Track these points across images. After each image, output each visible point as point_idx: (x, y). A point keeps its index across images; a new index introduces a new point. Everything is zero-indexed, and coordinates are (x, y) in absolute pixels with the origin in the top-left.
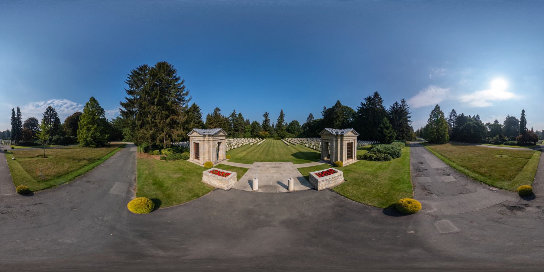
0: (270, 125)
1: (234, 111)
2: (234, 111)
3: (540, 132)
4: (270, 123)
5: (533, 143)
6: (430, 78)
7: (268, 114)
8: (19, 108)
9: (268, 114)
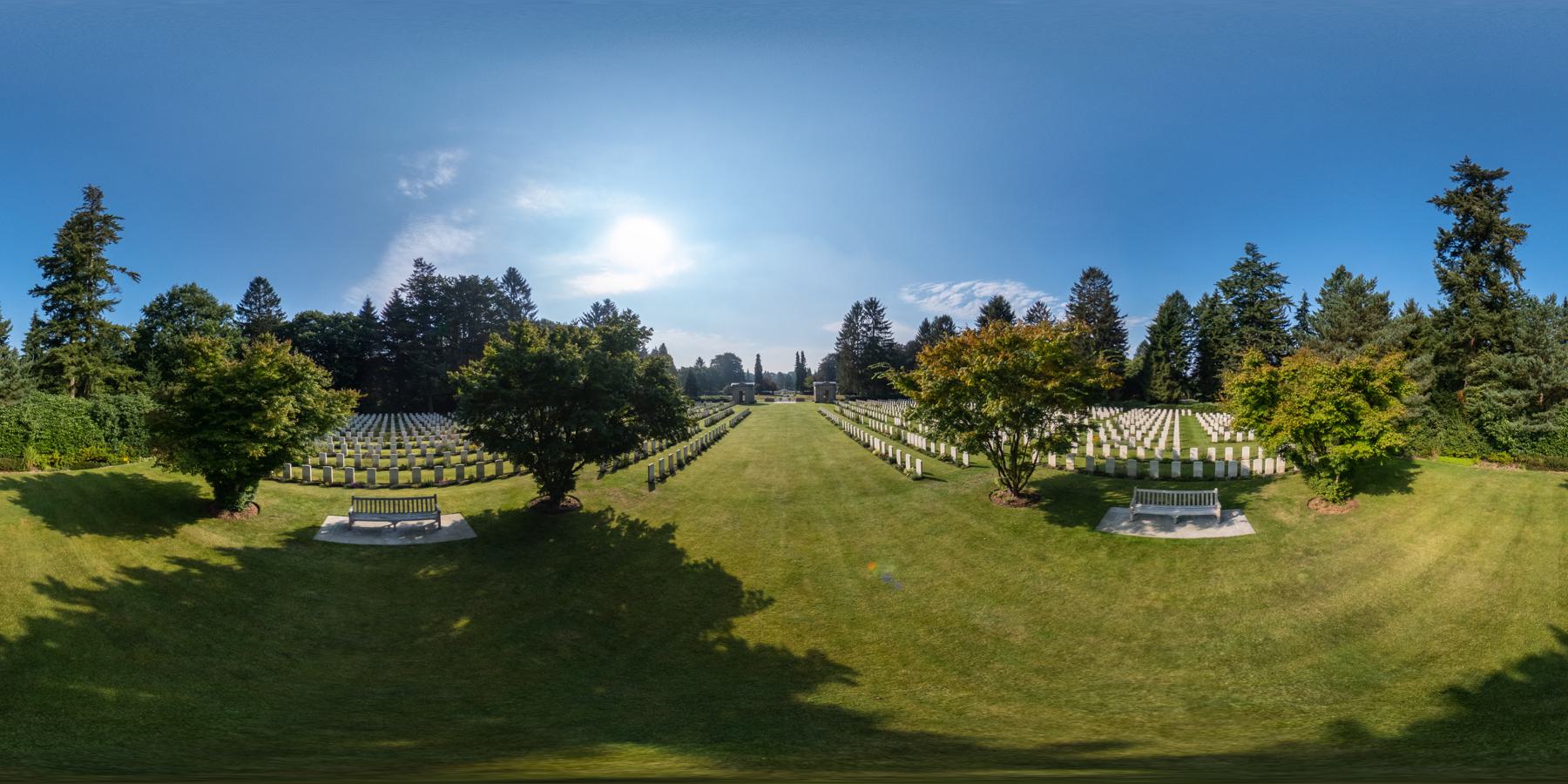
1: (1251, 249)
8: (173, 558)
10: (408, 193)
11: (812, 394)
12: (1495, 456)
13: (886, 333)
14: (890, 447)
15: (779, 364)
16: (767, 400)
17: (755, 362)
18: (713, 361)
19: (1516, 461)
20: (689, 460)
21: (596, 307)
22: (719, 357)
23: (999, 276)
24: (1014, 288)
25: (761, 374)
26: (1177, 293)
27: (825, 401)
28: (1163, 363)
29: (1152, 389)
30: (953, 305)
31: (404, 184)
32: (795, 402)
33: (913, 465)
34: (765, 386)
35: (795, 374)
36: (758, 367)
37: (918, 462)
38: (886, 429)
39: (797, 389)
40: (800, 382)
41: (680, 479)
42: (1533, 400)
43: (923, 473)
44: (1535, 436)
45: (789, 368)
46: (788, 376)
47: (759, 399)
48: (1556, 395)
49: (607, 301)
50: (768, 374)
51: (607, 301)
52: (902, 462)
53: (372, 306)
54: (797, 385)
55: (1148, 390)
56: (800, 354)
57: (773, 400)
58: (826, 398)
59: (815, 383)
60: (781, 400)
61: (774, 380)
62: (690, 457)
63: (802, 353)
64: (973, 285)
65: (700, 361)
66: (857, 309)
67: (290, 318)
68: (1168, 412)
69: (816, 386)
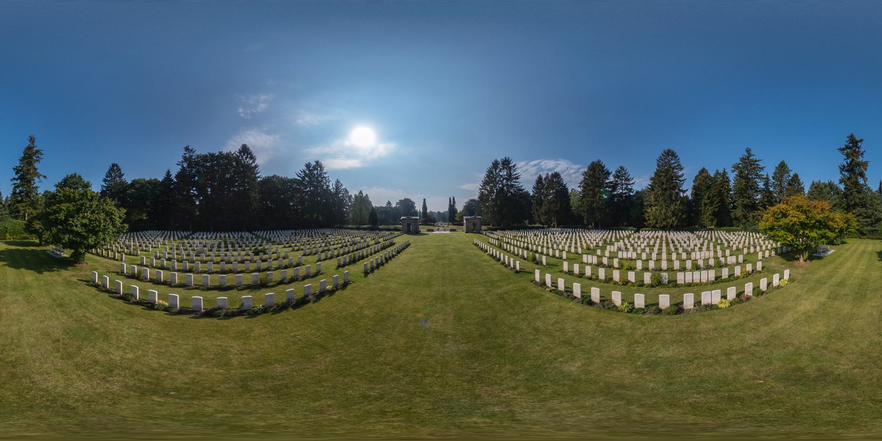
1: (748, 151)
2: (748, 151)
4: (867, 174)
8: (454, 202)
10: (242, 115)
11: (462, 225)
13: (516, 182)
14: (498, 252)
15: (438, 206)
16: (428, 230)
17: (422, 204)
21: (308, 166)
22: (401, 201)
23: (555, 157)
24: (565, 163)
25: (427, 213)
27: (472, 232)
28: (708, 207)
29: (701, 220)
30: (531, 174)
31: (241, 110)
32: (449, 232)
34: (429, 219)
35: (448, 213)
36: (425, 208)
37: (518, 263)
38: (512, 249)
40: (452, 217)
41: (389, 266)
42: (872, 221)
43: (520, 269)
45: (444, 208)
46: (444, 214)
47: (423, 229)
48: (878, 220)
49: (317, 162)
50: (431, 212)
51: (317, 162)
52: (508, 263)
53: (171, 174)
54: (450, 219)
55: (699, 221)
56: (452, 199)
57: (432, 231)
58: (474, 229)
59: (465, 217)
60: (438, 230)
61: (435, 216)
63: (454, 198)
64: (541, 162)
65: (389, 203)
66: (495, 165)
67: (130, 182)
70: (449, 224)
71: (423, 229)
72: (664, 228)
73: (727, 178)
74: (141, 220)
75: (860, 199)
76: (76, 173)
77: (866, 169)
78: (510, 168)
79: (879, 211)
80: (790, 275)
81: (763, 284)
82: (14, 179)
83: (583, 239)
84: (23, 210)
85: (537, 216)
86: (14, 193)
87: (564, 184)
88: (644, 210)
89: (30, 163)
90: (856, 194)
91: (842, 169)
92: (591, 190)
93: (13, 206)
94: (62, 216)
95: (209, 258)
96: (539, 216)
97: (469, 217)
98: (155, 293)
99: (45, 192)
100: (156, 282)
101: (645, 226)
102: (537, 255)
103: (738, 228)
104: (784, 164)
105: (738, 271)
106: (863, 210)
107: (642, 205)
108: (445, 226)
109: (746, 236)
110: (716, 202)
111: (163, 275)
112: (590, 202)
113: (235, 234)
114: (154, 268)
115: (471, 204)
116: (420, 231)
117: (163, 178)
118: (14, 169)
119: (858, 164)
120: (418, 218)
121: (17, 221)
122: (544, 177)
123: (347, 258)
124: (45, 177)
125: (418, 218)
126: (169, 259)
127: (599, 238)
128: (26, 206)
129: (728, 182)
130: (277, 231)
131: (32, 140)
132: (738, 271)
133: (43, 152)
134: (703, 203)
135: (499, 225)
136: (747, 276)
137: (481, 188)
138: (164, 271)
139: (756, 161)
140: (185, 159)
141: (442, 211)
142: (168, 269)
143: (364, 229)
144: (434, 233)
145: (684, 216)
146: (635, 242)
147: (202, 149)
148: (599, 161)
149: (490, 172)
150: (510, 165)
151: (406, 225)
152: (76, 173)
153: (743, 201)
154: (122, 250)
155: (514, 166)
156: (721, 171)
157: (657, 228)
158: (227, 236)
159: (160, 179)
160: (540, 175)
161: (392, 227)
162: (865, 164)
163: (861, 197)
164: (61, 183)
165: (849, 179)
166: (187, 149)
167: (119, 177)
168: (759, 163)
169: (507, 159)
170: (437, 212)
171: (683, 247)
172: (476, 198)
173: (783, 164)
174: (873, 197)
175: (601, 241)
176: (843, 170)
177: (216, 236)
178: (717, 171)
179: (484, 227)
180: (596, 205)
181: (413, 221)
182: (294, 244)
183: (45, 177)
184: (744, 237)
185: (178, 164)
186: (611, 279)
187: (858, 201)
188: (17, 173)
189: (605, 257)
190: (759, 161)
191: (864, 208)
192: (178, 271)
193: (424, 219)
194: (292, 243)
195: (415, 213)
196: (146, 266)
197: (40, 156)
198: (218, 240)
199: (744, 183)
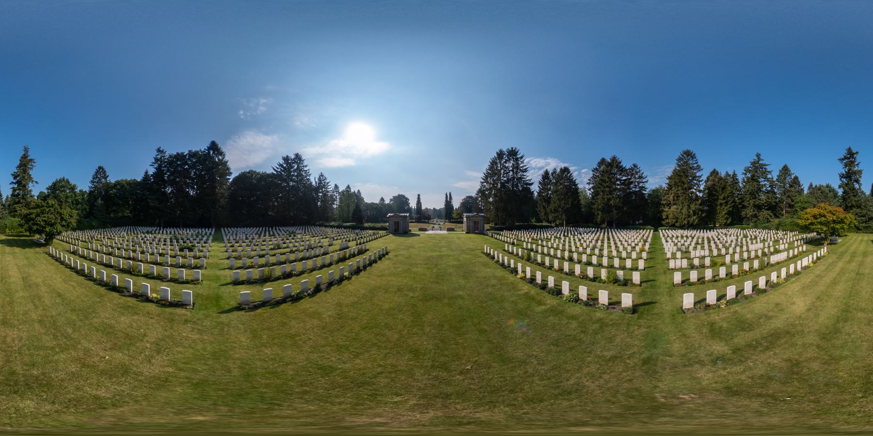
0: (863, 188)
1: (758, 155)
2: (758, 155)
3: (430, 209)
4: (862, 181)
5: (427, 221)
6: (242, 117)
7: (857, 153)
8: (451, 198)
9: (857, 153)
11: (462, 222)
12: (859, 231)
15: (433, 202)
16: (421, 230)
17: (416, 200)
18: (391, 200)
19: (863, 233)
20: (342, 279)
22: (395, 198)
26: (715, 170)
28: (723, 206)
32: (445, 232)
33: (524, 272)
34: (423, 217)
36: (419, 203)
39: (446, 219)
40: (449, 214)
44: (867, 227)
45: (440, 205)
46: (440, 210)
47: (414, 228)
48: (871, 219)
50: (426, 209)
52: (502, 261)
56: (448, 195)
57: (425, 230)
58: (475, 229)
59: (465, 215)
60: (433, 229)
61: (430, 213)
62: (345, 276)
65: (382, 199)
66: (500, 155)
68: (650, 231)
69: (467, 217)
70: (445, 222)
71: (414, 228)
72: (682, 227)
73: (737, 179)
74: (124, 217)
75: (856, 201)
76: (64, 177)
77: (860, 177)
78: (517, 159)
79: (872, 211)
80: (787, 272)
81: (762, 282)
82: (12, 183)
83: (612, 240)
84: (20, 210)
85: (543, 214)
86: (13, 195)
87: (574, 179)
88: (661, 209)
89: (25, 171)
90: (852, 198)
91: (842, 176)
92: (608, 187)
93: (12, 206)
94: (33, 216)
95: (201, 254)
96: (546, 214)
97: (470, 214)
98: (148, 285)
99: (40, 193)
100: (147, 276)
101: (663, 226)
102: (532, 254)
103: (748, 226)
104: (787, 167)
105: (735, 269)
106: (858, 210)
107: (659, 204)
108: (441, 223)
109: (770, 233)
110: (731, 202)
111: (156, 270)
112: (606, 199)
113: (180, 230)
114: (148, 263)
115: (469, 201)
116: (410, 231)
117: (142, 178)
118: (13, 175)
119: (855, 173)
120: (408, 214)
121: (15, 219)
122: (550, 172)
123: (255, 273)
124: (37, 182)
125: (408, 214)
126: (152, 254)
127: (638, 238)
128: (22, 206)
129: (737, 183)
130: (226, 229)
131: (26, 150)
132: (735, 269)
133: (35, 161)
134: (719, 203)
135: (503, 224)
136: (743, 274)
137: (482, 181)
138: (158, 266)
139: (765, 165)
140: (156, 160)
141: (438, 208)
142: (160, 264)
143: (345, 227)
144: (427, 232)
145: (703, 215)
146: (678, 242)
147: (171, 151)
148: (614, 159)
149: (493, 163)
150: (518, 156)
151: (393, 223)
152: (64, 177)
153: (755, 202)
154: (122, 246)
155: (522, 157)
156: (731, 173)
157: (676, 227)
158: (200, 231)
159: (139, 179)
160: (547, 169)
161: (379, 225)
162: (860, 172)
163: (856, 200)
164: (51, 186)
165: (847, 185)
166: (159, 150)
167: (104, 178)
168: (767, 167)
169: (514, 149)
170: (432, 209)
171: (623, 245)
172: (473, 194)
173: (786, 168)
174: (867, 200)
175: (640, 242)
176: (842, 177)
177: (167, 232)
178: (727, 172)
179: (487, 226)
180: (613, 203)
181: (401, 218)
182: (245, 244)
183: (37, 182)
184: (769, 234)
185: (151, 165)
186: (562, 270)
187: (854, 203)
188: (14, 178)
189: (595, 255)
190: (768, 165)
191: (859, 209)
192: (172, 266)
193: (418, 216)
194: (287, 240)
195: (409, 210)
196: (141, 261)
197: (33, 164)
198: (165, 236)
199: (756, 186)
